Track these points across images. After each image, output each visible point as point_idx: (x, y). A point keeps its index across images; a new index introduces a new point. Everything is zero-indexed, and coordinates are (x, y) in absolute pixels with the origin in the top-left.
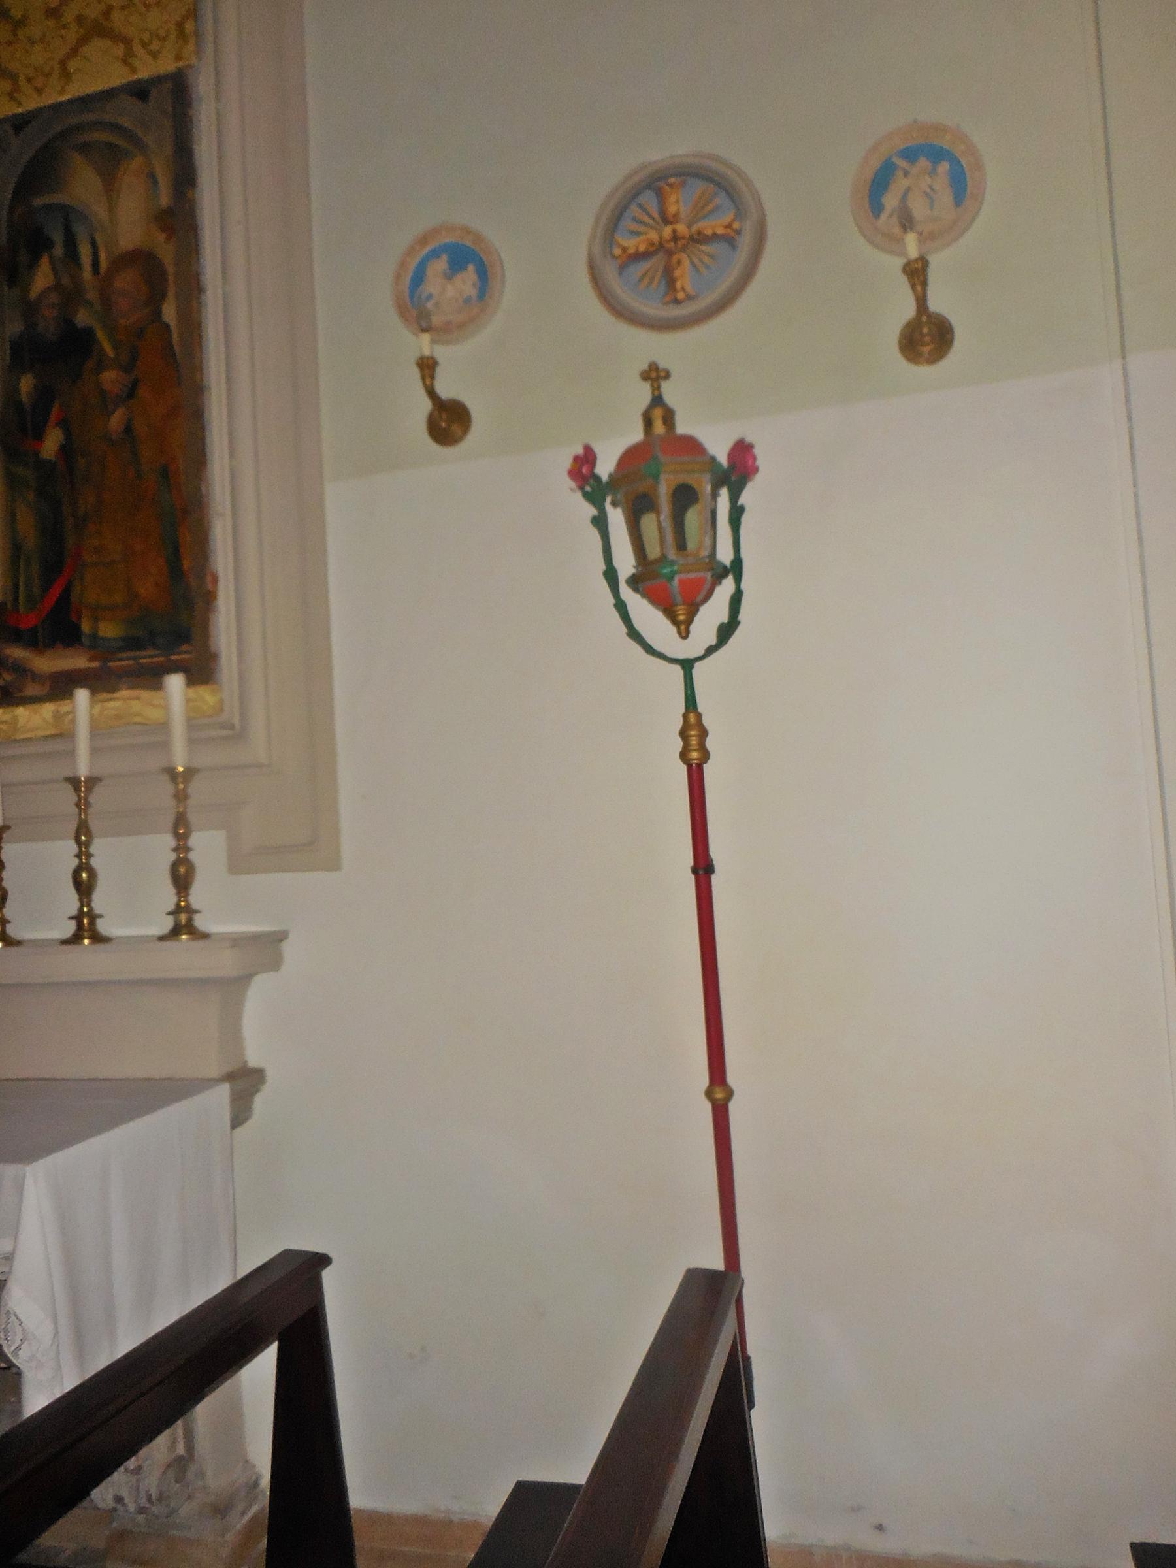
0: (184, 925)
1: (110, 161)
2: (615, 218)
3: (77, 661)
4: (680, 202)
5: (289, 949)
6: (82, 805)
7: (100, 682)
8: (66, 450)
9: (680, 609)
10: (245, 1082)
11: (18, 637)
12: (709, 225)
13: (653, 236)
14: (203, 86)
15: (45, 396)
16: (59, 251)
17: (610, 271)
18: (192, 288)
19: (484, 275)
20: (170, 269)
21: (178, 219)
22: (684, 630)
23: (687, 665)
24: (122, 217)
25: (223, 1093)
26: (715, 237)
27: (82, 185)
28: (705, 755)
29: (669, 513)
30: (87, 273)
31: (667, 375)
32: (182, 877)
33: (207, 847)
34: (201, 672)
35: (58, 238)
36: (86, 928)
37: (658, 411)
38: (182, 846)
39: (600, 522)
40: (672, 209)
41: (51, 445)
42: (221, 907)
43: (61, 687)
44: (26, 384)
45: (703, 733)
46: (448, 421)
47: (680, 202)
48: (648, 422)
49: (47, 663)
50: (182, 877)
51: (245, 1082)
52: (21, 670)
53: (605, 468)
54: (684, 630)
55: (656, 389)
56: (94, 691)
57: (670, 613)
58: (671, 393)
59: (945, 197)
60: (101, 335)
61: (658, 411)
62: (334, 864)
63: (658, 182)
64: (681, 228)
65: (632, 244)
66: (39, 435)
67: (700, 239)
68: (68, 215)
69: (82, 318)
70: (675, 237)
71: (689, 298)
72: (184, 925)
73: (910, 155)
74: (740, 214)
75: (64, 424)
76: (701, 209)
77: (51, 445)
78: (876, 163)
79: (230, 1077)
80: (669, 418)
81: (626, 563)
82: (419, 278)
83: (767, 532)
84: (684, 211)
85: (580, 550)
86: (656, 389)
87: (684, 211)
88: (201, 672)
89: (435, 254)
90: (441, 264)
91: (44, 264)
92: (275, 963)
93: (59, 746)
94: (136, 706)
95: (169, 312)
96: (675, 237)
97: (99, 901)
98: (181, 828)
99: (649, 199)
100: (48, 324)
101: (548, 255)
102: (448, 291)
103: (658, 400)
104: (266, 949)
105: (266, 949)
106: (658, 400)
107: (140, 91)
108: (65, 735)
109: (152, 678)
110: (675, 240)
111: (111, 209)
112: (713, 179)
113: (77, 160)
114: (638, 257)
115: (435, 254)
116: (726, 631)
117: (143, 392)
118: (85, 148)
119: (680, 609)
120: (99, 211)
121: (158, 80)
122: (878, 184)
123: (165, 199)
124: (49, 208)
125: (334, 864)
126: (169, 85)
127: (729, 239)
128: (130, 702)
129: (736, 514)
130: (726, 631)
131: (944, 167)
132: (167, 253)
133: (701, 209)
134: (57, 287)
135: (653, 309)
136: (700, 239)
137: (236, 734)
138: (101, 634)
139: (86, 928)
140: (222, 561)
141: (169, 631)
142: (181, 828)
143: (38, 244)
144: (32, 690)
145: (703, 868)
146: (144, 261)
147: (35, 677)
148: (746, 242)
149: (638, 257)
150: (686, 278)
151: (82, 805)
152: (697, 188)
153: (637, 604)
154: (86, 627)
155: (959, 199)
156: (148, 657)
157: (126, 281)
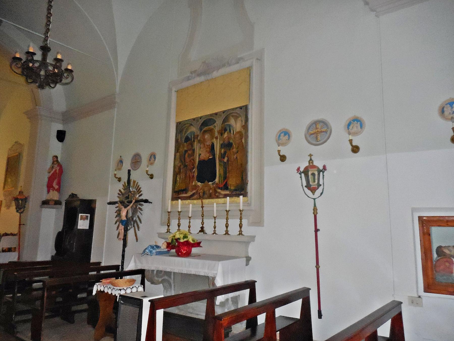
0: (241, 233)
1: (236, 118)
2: (309, 128)
3: (227, 192)
4: (319, 126)
5: (256, 239)
6: (227, 214)
7: (230, 196)
8: (228, 160)
9: (313, 190)
10: (248, 259)
11: (219, 188)
12: (323, 130)
13: (315, 131)
14: (250, 107)
15: (225, 153)
16: (228, 131)
17: (308, 136)
18: (247, 137)
19: (289, 136)
20: (244, 134)
21: (245, 127)
22: (314, 194)
23: (314, 199)
24: (237, 125)
25: (245, 259)
26: (323, 132)
27: (232, 122)
28: (317, 213)
29: (312, 177)
30: (232, 134)
31: (312, 155)
32: (241, 226)
33: (244, 222)
34: (245, 195)
35: (228, 129)
36: (227, 233)
37: (311, 161)
38: (241, 222)
39: (301, 177)
40: (318, 127)
41: (226, 160)
42: (247, 230)
43: (225, 196)
44: (223, 151)
45: (317, 210)
46: (283, 158)
47: (319, 126)
48: (309, 163)
49: (224, 192)
50: (241, 226)
51: (248, 259)
52: (220, 193)
53: (302, 169)
54: (314, 194)
55: (311, 157)
56: (230, 197)
57: (312, 191)
58: (312, 158)
59: (359, 127)
60: (233, 144)
61: (311, 161)
62: (263, 226)
63: (316, 123)
64: (319, 130)
65: (312, 132)
66: (224, 158)
67: (322, 132)
68: (230, 126)
69: (231, 141)
70: (318, 131)
71: (320, 141)
72: (241, 233)
73: (354, 120)
74: (328, 128)
75: (228, 157)
76: (322, 127)
77: (226, 160)
78: (348, 122)
79: (246, 257)
80: (312, 163)
81: (305, 184)
82: (280, 136)
83: (327, 179)
84: (319, 127)
85: (299, 181)
86: (311, 157)
87: (319, 127)
88: (245, 195)
89: (281, 133)
90: (283, 134)
91: (226, 133)
92: (254, 241)
93: (224, 205)
94: (235, 200)
95: (243, 141)
96: (318, 131)
97: (229, 229)
98: (241, 219)
99: (314, 125)
100: (226, 142)
101: (299, 135)
102: (284, 138)
103: (311, 160)
104: (252, 238)
105: (252, 238)
106: (311, 160)
107: (241, 108)
108: (225, 203)
109: (238, 195)
110: (318, 132)
111: (236, 125)
112: (324, 123)
113: (231, 117)
114: (312, 134)
115: (281, 133)
116: (321, 194)
117: (239, 152)
118: (232, 116)
119: (313, 190)
120: (235, 126)
121: (243, 106)
122: (349, 125)
123: (243, 124)
124: (227, 124)
125: (263, 226)
126: (244, 108)
127: (326, 132)
128: (235, 199)
129: (323, 176)
130: (321, 194)
131: (359, 123)
132: (243, 132)
133: (322, 127)
134: (228, 136)
135: (315, 143)
136: (322, 132)
137: (249, 205)
138: (52, 67)
139: (227, 233)
140: (249, 150)
141: (241, 190)
142: (241, 219)
143: (225, 130)
144: (221, 196)
145: (317, 230)
146: (240, 133)
147: (222, 194)
148: (328, 133)
149: (312, 134)
150: (319, 138)
151: (227, 214)
152: (321, 124)
153: (306, 189)
154: (229, 187)
155: (361, 128)
156: (238, 192)
157: (238, 136)
